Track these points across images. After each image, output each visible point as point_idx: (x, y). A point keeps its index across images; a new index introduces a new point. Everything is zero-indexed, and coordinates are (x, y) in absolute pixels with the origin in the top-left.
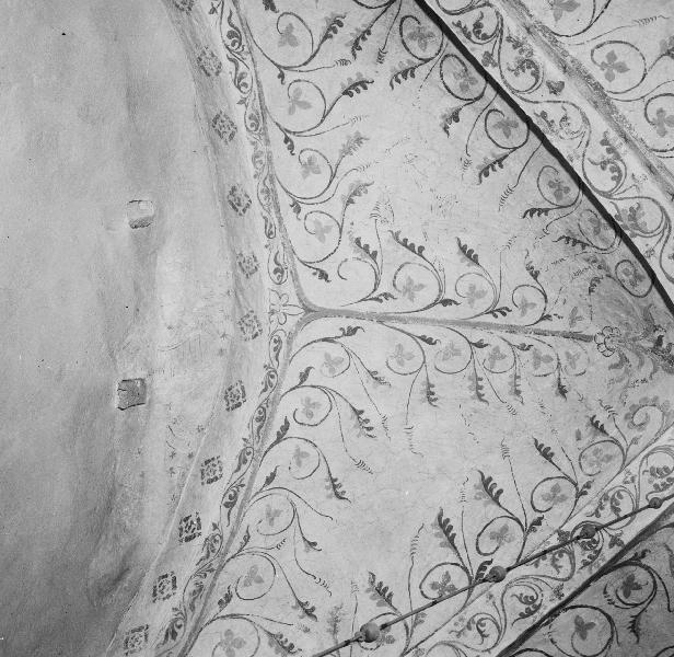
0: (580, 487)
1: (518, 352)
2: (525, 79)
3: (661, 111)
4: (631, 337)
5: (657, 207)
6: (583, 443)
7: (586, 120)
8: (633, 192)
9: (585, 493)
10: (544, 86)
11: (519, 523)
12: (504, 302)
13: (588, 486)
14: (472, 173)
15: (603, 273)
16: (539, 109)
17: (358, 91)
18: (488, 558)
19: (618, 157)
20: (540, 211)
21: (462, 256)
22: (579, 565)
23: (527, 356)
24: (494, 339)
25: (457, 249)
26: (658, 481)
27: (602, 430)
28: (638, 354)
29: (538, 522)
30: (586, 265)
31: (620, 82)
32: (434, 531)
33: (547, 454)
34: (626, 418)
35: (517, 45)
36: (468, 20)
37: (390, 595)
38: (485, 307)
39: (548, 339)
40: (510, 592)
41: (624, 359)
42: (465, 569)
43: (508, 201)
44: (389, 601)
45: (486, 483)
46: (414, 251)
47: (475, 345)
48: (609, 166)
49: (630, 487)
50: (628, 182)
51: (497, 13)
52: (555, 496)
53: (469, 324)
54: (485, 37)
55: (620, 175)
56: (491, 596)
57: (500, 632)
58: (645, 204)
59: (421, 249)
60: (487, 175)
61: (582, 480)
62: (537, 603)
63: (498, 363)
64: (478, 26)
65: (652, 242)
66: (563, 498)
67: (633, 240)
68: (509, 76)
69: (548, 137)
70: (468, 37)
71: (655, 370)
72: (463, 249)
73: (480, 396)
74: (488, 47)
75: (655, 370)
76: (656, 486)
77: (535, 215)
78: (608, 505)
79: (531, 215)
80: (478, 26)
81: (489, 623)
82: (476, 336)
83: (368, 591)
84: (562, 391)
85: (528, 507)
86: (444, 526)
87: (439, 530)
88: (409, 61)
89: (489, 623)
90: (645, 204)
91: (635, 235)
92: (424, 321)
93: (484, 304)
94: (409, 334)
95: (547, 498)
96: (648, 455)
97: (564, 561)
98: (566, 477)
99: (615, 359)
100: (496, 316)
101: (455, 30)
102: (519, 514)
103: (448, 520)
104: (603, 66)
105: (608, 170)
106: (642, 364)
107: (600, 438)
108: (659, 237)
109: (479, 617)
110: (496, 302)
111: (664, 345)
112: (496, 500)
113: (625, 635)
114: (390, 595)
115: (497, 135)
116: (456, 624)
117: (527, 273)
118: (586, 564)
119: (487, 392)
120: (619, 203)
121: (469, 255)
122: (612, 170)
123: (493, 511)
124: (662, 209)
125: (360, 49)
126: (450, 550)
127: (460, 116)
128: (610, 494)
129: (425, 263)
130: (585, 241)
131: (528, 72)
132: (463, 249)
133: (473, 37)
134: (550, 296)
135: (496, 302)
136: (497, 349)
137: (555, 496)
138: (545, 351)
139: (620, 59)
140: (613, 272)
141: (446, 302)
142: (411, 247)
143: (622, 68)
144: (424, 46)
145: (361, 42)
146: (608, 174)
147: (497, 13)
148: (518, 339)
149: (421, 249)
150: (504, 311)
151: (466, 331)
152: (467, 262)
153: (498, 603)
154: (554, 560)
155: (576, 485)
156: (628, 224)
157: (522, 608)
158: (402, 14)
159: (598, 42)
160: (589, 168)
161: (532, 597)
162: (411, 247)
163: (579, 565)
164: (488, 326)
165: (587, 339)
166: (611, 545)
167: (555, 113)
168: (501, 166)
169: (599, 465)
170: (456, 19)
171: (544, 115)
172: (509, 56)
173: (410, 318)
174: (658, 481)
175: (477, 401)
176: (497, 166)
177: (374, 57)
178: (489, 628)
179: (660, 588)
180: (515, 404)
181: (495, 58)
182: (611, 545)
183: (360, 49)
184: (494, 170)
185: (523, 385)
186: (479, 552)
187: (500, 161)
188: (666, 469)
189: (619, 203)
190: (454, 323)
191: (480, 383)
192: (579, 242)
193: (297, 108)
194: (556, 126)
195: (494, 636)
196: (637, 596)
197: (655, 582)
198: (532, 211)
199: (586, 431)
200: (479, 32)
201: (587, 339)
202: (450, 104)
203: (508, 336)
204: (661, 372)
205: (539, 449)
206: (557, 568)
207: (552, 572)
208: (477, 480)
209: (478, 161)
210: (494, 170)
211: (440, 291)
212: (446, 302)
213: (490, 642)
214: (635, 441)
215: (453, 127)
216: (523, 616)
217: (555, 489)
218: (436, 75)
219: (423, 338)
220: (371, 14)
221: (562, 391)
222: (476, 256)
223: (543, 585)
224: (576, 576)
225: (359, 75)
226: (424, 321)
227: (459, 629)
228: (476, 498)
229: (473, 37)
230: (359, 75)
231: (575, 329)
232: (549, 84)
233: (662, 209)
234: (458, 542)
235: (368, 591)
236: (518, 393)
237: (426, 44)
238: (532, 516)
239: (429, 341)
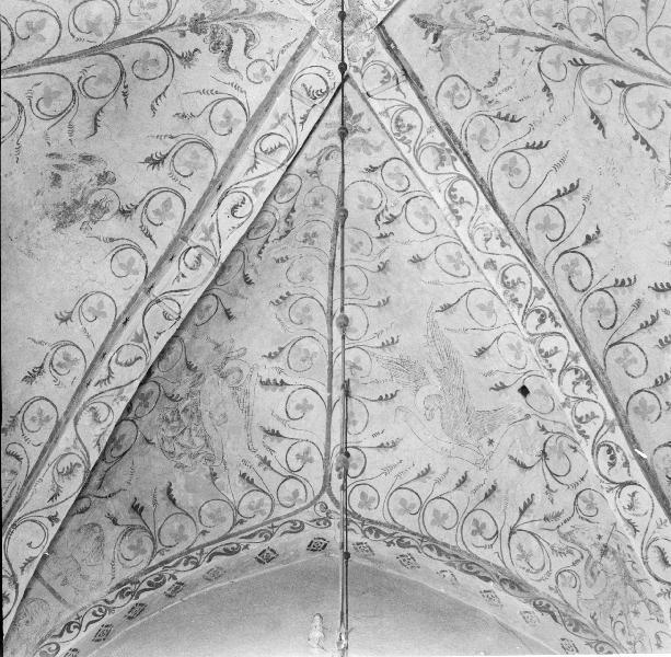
2: (512, 275)
3: (426, 223)
4: (464, 35)
7: (471, 237)
8: (441, 178)
10: (499, 267)
12: (574, 70)
14: (584, 189)
15: (484, 93)
16: (507, 250)
17: (662, 285)
19: (450, 206)
20: (533, 147)
21: (603, 121)
23: (558, 19)
24: (585, 40)
25: (607, 128)
28: (456, 21)
30: (499, 98)
31: (452, 249)
35: (515, 301)
36: (548, 326)
38: (588, 71)
39: (539, 30)
41: (469, 15)
43: (558, 159)
46: (642, 138)
48: (457, 200)
50: (444, 187)
51: (525, 327)
53: (605, 59)
54: (538, 311)
55: (449, 192)
58: (432, 170)
59: (636, 138)
60: (572, 185)
64: (542, 321)
65: (429, 139)
66: (144, 552)
67: (444, 141)
68: (525, 278)
69: (502, 226)
70: (551, 314)
71: (439, 12)
72: (601, 127)
74: (538, 303)
75: (439, 12)
77: (538, 143)
79: (541, 143)
80: (542, 321)
82: (599, 46)
88: (616, 292)
90: (432, 170)
91: (442, 144)
92: (642, 73)
93: (589, 74)
94: (657, 65)
99: (478, 15)
101: (561, 321)
104: (463, 263)
105: (459, 197)
106: (453, 15)
108: (424, 142)
110: (580, 73)
111: (431, 35)
115: (556, 219)
117: (552, 91)
120: (452, 170)
121: (596, 119)
122: (455, 196)
124: (420, 165)
125: (652, 316)
127: (584, 239)
129: (635, 125)
130: (496, 120)
131: (510, 280)
132: (601, 127)
133: (547, 312)
134: (534, 69)
135: (580, 73)
136: (584, 30)
138: (542, 20)
139: (452, 265)
140: (474, 94)
141: (620, 84)
142: (644, 142)
143: (450, 258)
144: (601, 302)
145: (650, 321)
146: (459, 194)
147: (525, 327)
148: (565, 35)
149: (636, 138)
150: (575, 63)
151: (608, 54)
152: (599, 115)
156: (446, 154)
158: (611, 332)
159: (465, 280)
160: (474, 201)
162: (644, 142)
164: (589, 53)
165: (502, 30)
167: (495, 245)
168: (559, 191)
170: (558, 330)
171: (503, 244)
172: (522, 294)
173: (655, 79)
176: (562, 191)
177: (644, 306)
181: (533, 294)
183: (652, 316)
184: (565, 189)
187: (559, 195)
189: (452, 170)
190: (615, 63)
192: (502, 119)
194: (495, 234)
198: (540, 146)
200: (542, 316)
201: (502, 30)
202: (589, 251)
203: (573, 39)
204: (433, 13)
207: (415, 132)
209: (578, 198)
210: (565, 189)
211: (625, 97)
212: (620, 84)
215: (592, 232)
218: (597, 277)
219: (646, 58)
220: (634, 339)
222: (592, 118)
225: (658, 298)
226: (642, 73)
229: (547, 312)
230: (658, 298)
231: (515, 38)
232: (496, 268)
233: (420, 165)
237: (598, 304)
239: (640, 53)
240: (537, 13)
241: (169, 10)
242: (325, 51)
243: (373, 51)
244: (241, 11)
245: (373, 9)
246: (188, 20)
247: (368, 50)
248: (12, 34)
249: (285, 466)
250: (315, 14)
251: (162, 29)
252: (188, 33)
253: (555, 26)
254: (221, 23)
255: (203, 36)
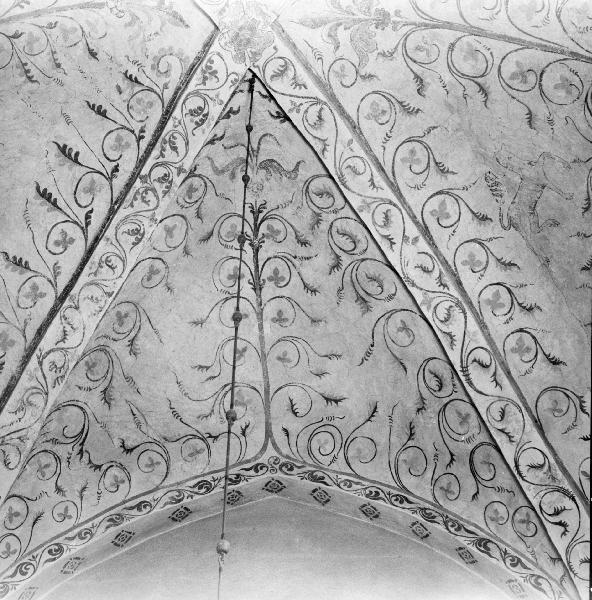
0: (137, 132)
1: (48, 31)
5: (477, 387)
6: (125, 96)
9: (143, 137)
11: (101, 174)
13: (142, 131)
18: (89, 209)
22: (161, 195)
26: (197, 119)
27: (136, 81)
29: (116, 169)
32: (39, 202)
33: (101, 112)
34: (153, 67)
37: (26, 263)
39: (69, 13)
40: (120, 231)
42: (76, 223)
44: (27, 267)
45: (64, 150)
47: (14, 37)
49: (179, 129)
52: (120, 145)
56: (108, 239)
57: (123, 261)
61: (137, 127)
62: (142, 231)
63: (35, 45)
66: (128, 145)
73: (30, 78)
76: (197, 123)
78: (168, 147)
81: (113, 258)
83: (7, 267)
84: (93, 54)
85: (103, 160)
86: (45, 195)
87: (43, 200)
89: (113, 258)
95: (115, 148)
96: (184, 103)
97: (150, 196)
98: (123, 127)
100: (22, 7)
102: (99, 167)
103: (46, 190)
107: (138, 88)
109: (105, 256)
112: (76, 161)
113: (195, 222)
114: (26, 263)
116: (91, 268)
118: (165, 193)
119: (34, 72)
123: (78, 171)
126: (57, 212)
128: (167, 138)
136: (31, 34)
137: (120, 145)
153: (114, 242)
154: (143, 198)
155: (133, 132)
157: (133, 239)
161: (137, 229)
163: (161, 195)
166: (179, 174)
169: (145, 112)
174: (197, 119)
175: (30, 84)
178: (115, 261)
179: (209, 184)
180: (60, 76)
182: (179, 174)
185: (61, 59)
186: (80, 206)
188: (200, 108)
191: (27, 68)
193: (279, 276)
195: (120, 265)
196: (196, 196)
197: (205, 183)
199: (124, 84)
205: (93, 109)
206: (147, 202)
207: (144, 206)
208: (55, 150)
213: (119, 270)
214: (166, 86)
216: (135, 244)
217: (119, 139)
221: (93, 54)
223: (140, 218)
224: (161, 203)
227: (94, 270)
228: (61, 165)
234: (60, 203)
235: (7, 267)
236: (58, 66)
238: (110, 166)
240: (76, 29)
241: (406, 39)
242: (265, 11)
243: (220, 13)
244: (342, 27)
245: (223, 52)
246: (390, 25)
247: (225, 14)
248: (541, 80)
249: (426, 173)
250: (275, 48)
251: (415, 24)
252: (392, 13)
253: (56, 23)
254: (362, 16)
255: (380, 7)
